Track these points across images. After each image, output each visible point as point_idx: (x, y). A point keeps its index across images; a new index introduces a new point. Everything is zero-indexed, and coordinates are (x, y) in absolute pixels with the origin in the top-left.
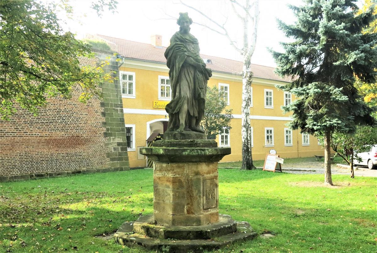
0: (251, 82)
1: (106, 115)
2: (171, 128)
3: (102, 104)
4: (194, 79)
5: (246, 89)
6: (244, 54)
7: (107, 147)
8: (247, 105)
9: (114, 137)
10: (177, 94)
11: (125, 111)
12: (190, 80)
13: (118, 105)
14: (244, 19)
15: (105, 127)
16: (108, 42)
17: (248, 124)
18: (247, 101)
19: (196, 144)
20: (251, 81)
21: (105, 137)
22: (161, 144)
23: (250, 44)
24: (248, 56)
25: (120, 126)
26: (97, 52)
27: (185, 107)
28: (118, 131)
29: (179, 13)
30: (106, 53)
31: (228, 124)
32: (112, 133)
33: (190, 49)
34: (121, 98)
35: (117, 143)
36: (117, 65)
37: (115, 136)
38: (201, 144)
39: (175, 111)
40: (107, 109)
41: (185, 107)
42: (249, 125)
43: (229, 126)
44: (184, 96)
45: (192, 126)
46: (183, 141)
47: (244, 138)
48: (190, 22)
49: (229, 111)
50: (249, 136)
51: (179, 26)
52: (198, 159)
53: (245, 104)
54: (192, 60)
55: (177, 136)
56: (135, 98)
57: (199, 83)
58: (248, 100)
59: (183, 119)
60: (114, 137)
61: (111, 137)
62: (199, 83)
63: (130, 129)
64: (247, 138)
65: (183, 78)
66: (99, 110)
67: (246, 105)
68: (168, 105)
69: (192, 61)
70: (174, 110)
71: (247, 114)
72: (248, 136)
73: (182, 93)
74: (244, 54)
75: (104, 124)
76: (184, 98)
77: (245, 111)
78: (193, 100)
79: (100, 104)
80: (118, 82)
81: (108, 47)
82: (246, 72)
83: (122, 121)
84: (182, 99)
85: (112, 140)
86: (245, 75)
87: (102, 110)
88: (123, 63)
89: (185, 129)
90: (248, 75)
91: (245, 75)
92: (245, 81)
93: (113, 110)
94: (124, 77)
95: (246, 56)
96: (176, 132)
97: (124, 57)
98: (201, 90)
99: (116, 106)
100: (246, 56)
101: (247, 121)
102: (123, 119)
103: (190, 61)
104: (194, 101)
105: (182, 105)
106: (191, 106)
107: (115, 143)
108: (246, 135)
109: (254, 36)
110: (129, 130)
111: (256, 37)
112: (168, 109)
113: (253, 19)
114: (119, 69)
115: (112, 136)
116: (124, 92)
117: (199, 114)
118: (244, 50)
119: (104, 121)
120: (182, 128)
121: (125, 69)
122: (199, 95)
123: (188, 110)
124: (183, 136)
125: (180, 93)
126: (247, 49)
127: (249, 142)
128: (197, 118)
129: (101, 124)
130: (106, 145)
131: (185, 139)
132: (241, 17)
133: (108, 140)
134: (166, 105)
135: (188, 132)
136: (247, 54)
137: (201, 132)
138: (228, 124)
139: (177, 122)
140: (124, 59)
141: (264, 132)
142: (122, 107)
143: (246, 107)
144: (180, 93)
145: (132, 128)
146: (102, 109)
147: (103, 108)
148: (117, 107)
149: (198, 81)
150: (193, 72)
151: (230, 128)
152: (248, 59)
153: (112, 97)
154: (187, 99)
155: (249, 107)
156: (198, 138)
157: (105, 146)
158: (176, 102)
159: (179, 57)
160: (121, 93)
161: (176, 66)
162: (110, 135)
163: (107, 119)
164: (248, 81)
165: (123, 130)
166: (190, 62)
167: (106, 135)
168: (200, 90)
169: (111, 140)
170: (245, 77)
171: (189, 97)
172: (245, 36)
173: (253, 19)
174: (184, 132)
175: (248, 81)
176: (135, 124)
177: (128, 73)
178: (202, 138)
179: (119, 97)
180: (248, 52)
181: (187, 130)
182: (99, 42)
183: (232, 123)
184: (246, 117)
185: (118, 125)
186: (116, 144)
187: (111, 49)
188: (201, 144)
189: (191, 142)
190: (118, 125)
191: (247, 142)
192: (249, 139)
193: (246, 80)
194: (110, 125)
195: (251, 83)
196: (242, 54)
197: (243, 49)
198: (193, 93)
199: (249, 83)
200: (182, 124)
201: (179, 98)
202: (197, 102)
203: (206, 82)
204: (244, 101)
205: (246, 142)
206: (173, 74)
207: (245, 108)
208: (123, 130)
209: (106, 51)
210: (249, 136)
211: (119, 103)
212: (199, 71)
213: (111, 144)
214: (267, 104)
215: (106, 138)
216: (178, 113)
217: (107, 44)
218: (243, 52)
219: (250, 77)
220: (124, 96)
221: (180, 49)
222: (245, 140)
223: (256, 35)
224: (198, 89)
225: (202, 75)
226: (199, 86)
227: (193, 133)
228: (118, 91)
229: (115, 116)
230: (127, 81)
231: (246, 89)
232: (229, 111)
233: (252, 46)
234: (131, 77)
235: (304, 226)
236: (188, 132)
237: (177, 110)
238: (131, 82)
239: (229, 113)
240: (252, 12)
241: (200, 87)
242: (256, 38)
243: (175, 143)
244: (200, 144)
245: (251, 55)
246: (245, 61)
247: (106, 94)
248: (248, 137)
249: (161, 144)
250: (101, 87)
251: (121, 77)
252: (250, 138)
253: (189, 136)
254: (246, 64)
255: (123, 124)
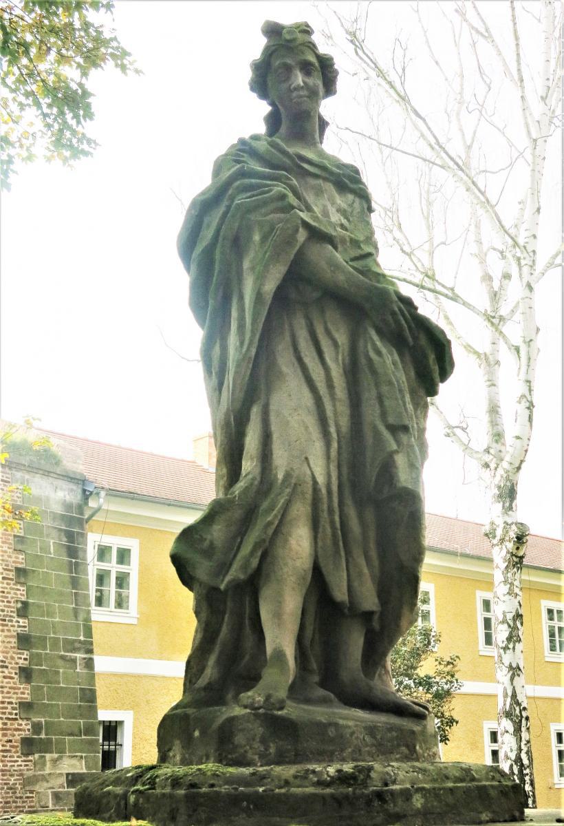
0: (522, 558)
1: (34, 676)
2: (209, 687)
3: (24, 641)
4: (353, 372)
5: (505, 582)
6: (493, 465)
7: (32, 792)
8: (513, 638)
9: (56, 756)
10: (249, 465)
11: (102, 663)
12: (330, 385)
13: (77, 645)
14: (487, 359)
15: (28, 719)
16: (55, 445)
17: (519, 704)
18: (512, 624)
19: (380, 795)
20: (521, 554)
21: (27, 755)
22: (125, 797)
23: (511, 429)
24: (507, 472)
25: (82, 716)
26: (18, 470)
27: (299, 545)
28: (71, 734)
29: (260, 24)
30: (47, 473)
31: (446, 709)
32: (50, 741)
33: (326, 214)
34: (88, 620)
35: (68, 775)
36: (82, 514)
37: (61, 751)
38: (418, 802)
39: (235, 573)
40: (39, 655)
41: (299, 545)
42: (525, 709)
43: (447, 714)
44: (288, 476)
45: (345, 676)
46: (286, 771)
47: (507, 758)
48: (325, 71)
49: (449, 663)
50: (524, 749)
51: (265, 108)
52: (69, 480)
53: (506, 634)
54: (334, 263)
55: (239, 739)
56: (135, 621)
57: (380, 399)
58: (514, 619)
59: (281, 633)
60: (56, 756)
61: (48, 756)
62: (380, 399)
63: (116, 728)
64: (518, 759)
65: (285, 369)
66: (12, 658)
67: (509, 639)
68: (188, 535)
69: (336, 267)
70: (224, 567)
71: (515, 671)
72: (520, 750)
73: (281, 460)
74: (493, 465)
75: (26, 707)
76: (295, 487)
77: (508, 658)
78: (349, 502)
79: (15, 640)
80: (81, 567)
81: (54, 456)
82: (502, 525)
83: (89, 697)
84: (275, 490)
85: (48, 764)
86: (499, 533)
87: (21, 661)
88: (99, 509)
89: (297, 690)
90: (512, 535)
91: (499, 533)
92: (500, 556)
93: (60, 662)
94: (103, 553)
95: (500, 472)
96: (237, 711)
97: (103, 488)
98: (398, 443)
99: (72, 646)
100: (500, 472)
101: (514, 696)
102: (93, 692)
103: (323, 264)
104: (352, 512)
105: (279, 531)
106: (335, 544)
107: (61, 774)
108: (515, 747)
109: (525, 404)
110: (111, 730)
111: (531, 407)
112: (190, 555)
113: (517, 350)
114: (87, 526)
115: (51, 752)
116: (99, 601)
117: (383, 593)
118: (492, 451)
119: (27, 697)
120: (277, 681)
121: (105, 528)
122: (387, 470)
123: (317, 570)
124: (286, 736)
125: (265, 456)
126: (503, 448)
127: (527, 771)
128: (376, 624)
129: (14, 709)
130: (29, 782)
131: (298, 758)
132: (476, 352)
133: (35, 764)
134: (179, 531)
135: (320, 713)
136: (505, 465)
137: (400, 710)
138: (446, 709)
139: (249, 641)
140: (103, 493)
141: (549, 739)
142: (90, 651)
143: (511, 646)
144: (265, 456)
145: (121, 723)
146: (22, 658)
147: (26, 654)
148: (75, 650)
149: (377, 385)
150: (342, 338)
151: (451, 722)
152: (508, 479)
153: (58, 618)
154: (309, 496)
155: (519, 646)
156: (384, 749)
157: (24, 785)
158: (238, 514)
159: (257, 237)
160: (89, 605)
161: (241, 298)
162: (45, 747)
163: (36, 691)
164: (512, 555)
165: (89, 730)
166: (327, 274)
167: (29, 745)
168: (386, 434)
169: (44, 764)
170: (502, 540)
171: (321, 480)
172: (494, 410)
173: (517, 350)
174: (292, 711)
175: (512, 555)
176: (132, 708)
177: (116, 542)
178: (412, 750)
179: (81, 616)
180: (508, 458)
181: (308, 701)
182: (26, 441)
183: (454, 708)
184: (512, 679)
185: (72, 713)
186: (63, 780)
187: (65, 462)
188: (418, 802)
189: (342, 778)
190: (72, 713)
191: (521, 771)
192: (526, 762)
193: (504, 552)
194: (45, 710)
195: (521, 562)
196: (487, 466)
197: (487, 451)
198: (345, 455)
199: (517, 562)
200: (279, 655)
201: (258, 492)
202: (370, 515)
203: (421, 407)
204: (504, 622)
205: (516, 771)
206: (224, 349)
207: (506, 648)
208: (89, 730)
209: (48, 468)
210: (524, 749)
211: (82, 638)
212: (380, 332)
213: (44, 778)
214: (553, 649)
215: (30, 758)
216: (251, 587)
217: (54, 449)
218: (487, 458)
219: (520, 539)
220: (97, 614)
221: (271, 190)
222: (511, 766)
223: (531, 403)
224: (377, 434)
225: (396, 357)
226: (384, 415)
227: (354, 718)
228: (79, 599)
229: (66, 680)
230: (113, 567)
231: (505, 582)
232: (449, 663)
233: (518, 438)
234: (123, 556)
235: (247, 739)
236: (320, 713)
237: (245, 567)
238: (123, 568)
239: (446, 669)
240: (514, 331)
241: (391, 420)
242: (531, 412)
243: (225, 789)
244: (407, 795)
245: (519, 468)
246: (499, 487)
247: (39, 606)
248: (524, 756)
249: (125, 797)
250: (22, 584)
251: (91, 553)
252: (530, 759)
253: (329, 742)
254: (500, 496)
255: (93, 710)
